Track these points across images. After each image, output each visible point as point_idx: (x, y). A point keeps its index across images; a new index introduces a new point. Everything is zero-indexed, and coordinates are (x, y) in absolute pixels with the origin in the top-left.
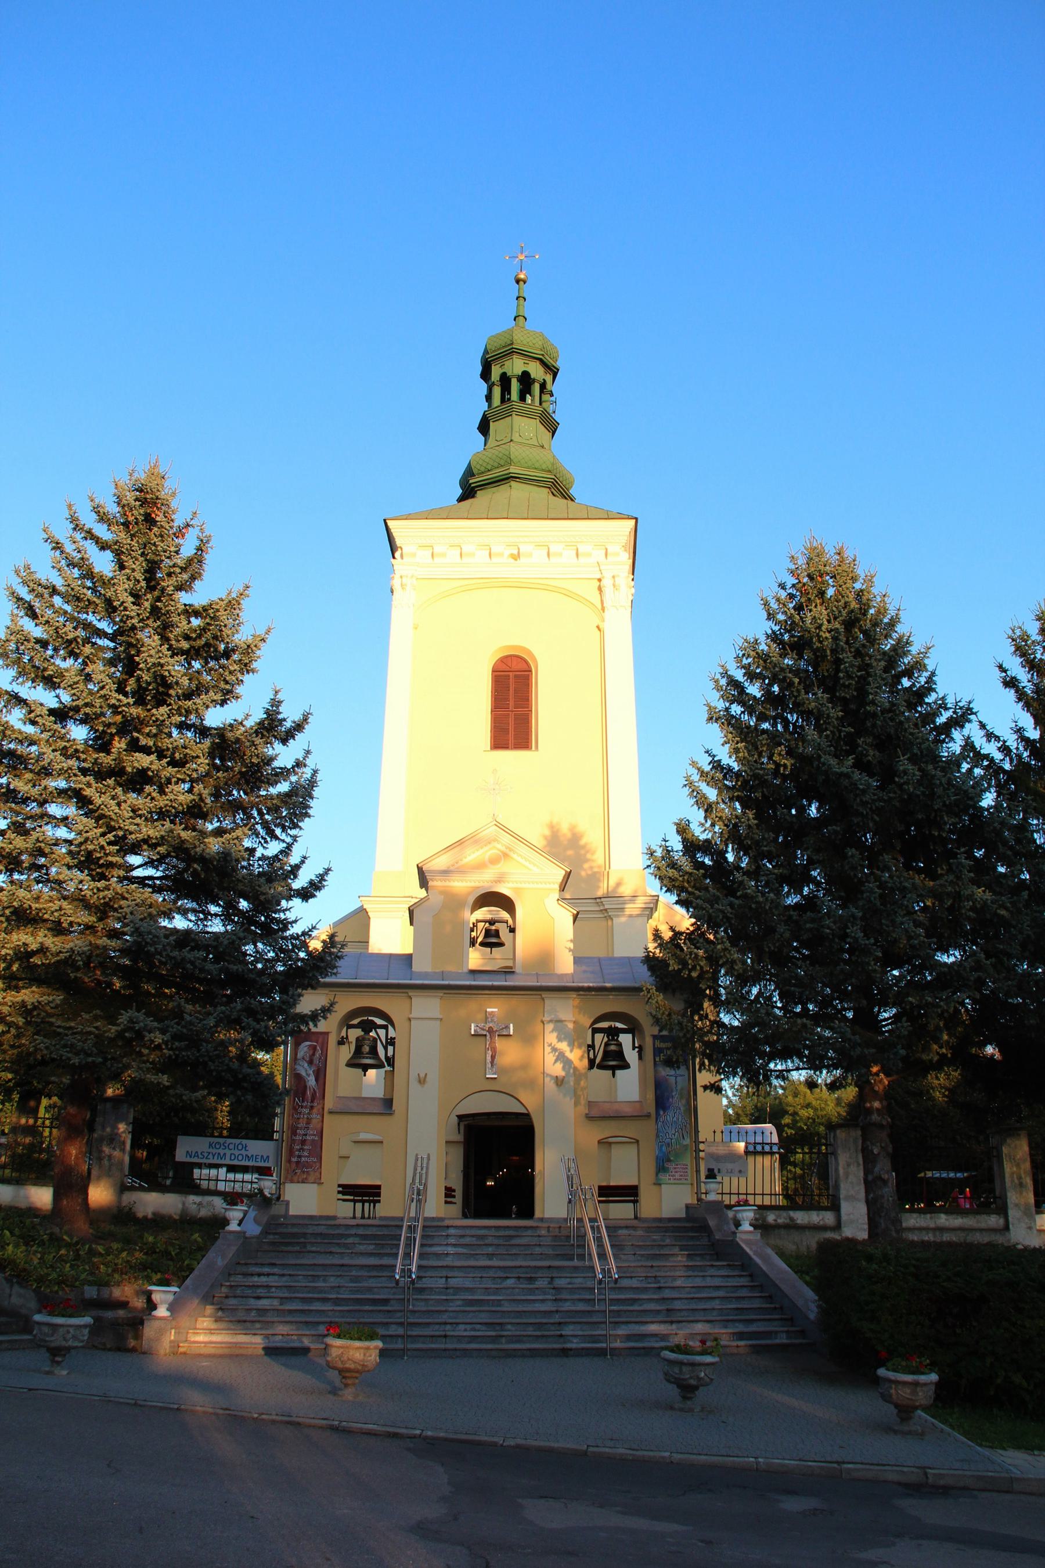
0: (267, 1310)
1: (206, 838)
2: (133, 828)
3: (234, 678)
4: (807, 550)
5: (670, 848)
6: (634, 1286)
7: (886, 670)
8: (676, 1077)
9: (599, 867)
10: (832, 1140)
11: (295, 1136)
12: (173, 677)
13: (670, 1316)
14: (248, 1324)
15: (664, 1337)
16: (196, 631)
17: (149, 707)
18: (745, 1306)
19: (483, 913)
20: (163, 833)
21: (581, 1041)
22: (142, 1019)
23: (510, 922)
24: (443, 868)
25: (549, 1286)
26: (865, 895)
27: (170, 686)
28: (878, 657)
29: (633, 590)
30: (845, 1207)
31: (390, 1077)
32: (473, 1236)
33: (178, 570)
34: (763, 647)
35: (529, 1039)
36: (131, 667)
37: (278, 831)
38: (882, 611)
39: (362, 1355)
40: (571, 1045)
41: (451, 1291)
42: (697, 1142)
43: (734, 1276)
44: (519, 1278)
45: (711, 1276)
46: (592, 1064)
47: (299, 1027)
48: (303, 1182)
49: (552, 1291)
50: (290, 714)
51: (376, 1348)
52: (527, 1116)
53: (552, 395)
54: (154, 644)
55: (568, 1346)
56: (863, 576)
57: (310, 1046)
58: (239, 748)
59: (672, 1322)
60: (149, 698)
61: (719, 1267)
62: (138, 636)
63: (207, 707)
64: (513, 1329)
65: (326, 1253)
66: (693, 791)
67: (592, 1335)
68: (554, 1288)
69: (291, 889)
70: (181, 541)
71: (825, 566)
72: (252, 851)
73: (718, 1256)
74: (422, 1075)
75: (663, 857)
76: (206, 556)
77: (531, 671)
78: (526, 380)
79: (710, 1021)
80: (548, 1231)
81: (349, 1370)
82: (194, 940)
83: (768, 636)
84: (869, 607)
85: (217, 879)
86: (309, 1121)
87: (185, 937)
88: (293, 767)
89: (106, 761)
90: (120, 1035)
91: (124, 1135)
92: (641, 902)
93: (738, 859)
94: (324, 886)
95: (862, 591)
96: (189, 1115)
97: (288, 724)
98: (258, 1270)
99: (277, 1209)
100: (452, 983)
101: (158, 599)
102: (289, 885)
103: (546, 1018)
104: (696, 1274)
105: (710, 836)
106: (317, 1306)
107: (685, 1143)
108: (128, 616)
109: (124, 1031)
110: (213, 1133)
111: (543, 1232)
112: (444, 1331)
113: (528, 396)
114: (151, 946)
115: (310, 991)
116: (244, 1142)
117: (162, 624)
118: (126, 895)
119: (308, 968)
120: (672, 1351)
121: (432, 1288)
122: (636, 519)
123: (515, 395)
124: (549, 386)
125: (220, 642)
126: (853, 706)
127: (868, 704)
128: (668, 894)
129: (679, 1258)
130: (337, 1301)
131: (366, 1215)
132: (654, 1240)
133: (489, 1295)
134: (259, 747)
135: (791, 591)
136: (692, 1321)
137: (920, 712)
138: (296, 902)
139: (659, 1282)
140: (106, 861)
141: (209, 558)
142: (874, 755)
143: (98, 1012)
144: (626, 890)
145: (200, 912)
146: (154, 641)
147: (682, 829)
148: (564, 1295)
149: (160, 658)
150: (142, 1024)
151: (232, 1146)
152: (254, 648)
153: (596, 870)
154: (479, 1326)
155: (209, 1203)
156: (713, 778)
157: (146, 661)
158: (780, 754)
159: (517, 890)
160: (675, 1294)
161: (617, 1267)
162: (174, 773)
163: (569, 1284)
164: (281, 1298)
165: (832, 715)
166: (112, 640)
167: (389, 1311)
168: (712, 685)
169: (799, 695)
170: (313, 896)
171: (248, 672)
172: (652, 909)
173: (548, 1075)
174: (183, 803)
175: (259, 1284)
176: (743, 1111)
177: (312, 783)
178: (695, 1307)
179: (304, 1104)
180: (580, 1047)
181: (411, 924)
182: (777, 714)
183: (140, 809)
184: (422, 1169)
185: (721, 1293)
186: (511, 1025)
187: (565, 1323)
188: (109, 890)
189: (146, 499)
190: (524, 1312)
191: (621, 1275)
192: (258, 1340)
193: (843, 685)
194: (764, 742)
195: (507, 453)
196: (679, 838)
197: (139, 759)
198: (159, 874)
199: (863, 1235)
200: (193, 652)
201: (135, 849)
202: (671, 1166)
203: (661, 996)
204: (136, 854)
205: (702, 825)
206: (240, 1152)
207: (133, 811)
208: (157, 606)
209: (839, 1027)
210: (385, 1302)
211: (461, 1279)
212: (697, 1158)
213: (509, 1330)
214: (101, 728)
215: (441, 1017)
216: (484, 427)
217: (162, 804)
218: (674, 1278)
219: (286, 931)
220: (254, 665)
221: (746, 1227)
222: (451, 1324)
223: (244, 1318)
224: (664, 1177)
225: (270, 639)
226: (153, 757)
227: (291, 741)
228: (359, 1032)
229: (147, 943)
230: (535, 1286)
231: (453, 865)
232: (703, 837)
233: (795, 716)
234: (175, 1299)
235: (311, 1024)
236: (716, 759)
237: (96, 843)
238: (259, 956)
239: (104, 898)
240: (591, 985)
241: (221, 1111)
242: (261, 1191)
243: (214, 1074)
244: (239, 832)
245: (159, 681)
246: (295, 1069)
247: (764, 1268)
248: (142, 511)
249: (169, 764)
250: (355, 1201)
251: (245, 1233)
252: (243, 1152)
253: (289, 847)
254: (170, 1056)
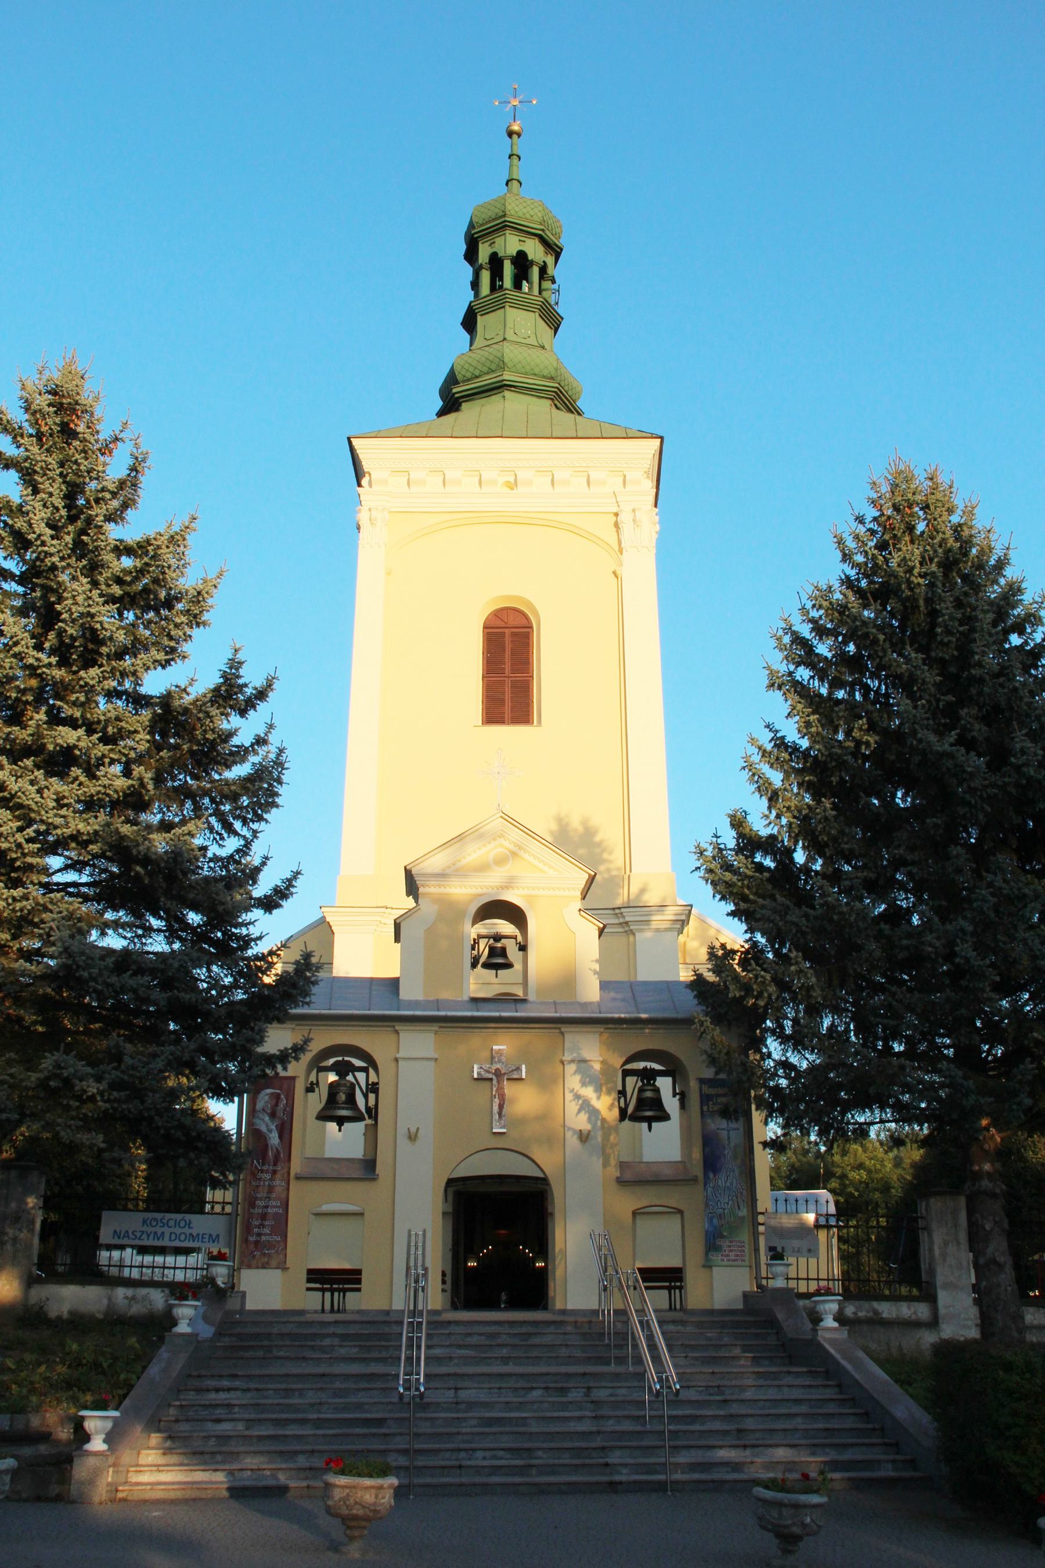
0: (230, 1437)
1: (152, 833)
2: (59, 821)
3: (181, 633)
4: (892, 474)
5: (722, 846)
6: (693, 1398)
7: (995, 624)
8: (729, 1131)
9: (618, 869)
10: (924, 1212)
11: (254, 1208)
12: (106, 630)
13: (741, 1438)
14: (207, 1457)
15: (737, 1467)
16: (131, 573)
17: (75, 668)
18: (836, 1426)
19: (481, 928)
20: (97, 827)
21: (609, 1085)
22: (74, 1065)
23: (520, 938)
24: (436, 871)
25: (586, 1399)
26: (975, 905)
27: (102, 642)
28: (986, 608)
29: (657, 528)
30: (943, 1297)
31: (372, 1135)
32: (481, 1334)
33: (108, 496)
34: (838, 596)
35: (548, 1082)
36: (49, 618)
37: (238, 825)
38: (986, 551)
39: (373, 1496)
40: (598, 1090)
41: (463, 1406)
42: (754, 1213)
43: (818, 1386)
44: (547, 1388)
45: (789, 1386)
46: (623, 1114)
47: (264, 1071)
48: (264, 1267)
49: (589, 1405)
50: (252, 677)
51: (390, 1486)
52: (545, 1180)
53: (554, 282)
54: (80, 590)
55: (617, 1478)
56: (961, 506)
57: (272, 1094)
58: (186, 720)
59: (745, 1447)
60: (74, 657)
61: (798, 1374)
62: (60, 579)
63: (148, 668)
64: (545, 1456)
65: (297, 1358)
66: (754, 775)
67: (645, 1464)
68: (592, 1402)
69: (251, 898)
70: (108, 459)
71: (914, 494)
72: (204, 849)
73: (791, 1360)
74: (413, 1130)
75: (714, 858)
76: (142, 479)
77: (531, 627)
78: (521, 261)
79: (774, 1060)
80: (576, 1327)
81: (356, 1518)
82: (135, 962)
83: (842, 582)
84: (972, 546)
85: (164, 885)
86: (271, 1189)
87: (124, 960)
88: (252, 745)
89: (21, 737)
90: (43, 1084)
91: (33, 1212)
92: (670, 914)
93: (810, 859)
94: (292, 894)
95: (960, 525)
96: (96, 1183)
97: (249, 691)
98: (212, 1383)
99: (232, 1304)
100: (450, 1013)
101: (83, 532)
102: (249, 893)
103: (567, 1057)
104: (769, 1382)
105: (775, 831)
106: (291, 1430)
107: (741, 1214)
108: (46, 553)
109: (48, 1079)
110: (126, 1205)
111: (569, 1328)
112: (457, 1459)
113: (525, 283)
114: (84, 970)
115: (275, 1025)
116: (188, 1217)
117: (90, 563)
118: (50, 906)
119: (278, 996)
120: (767, 1487)
121: (438, 1404)
122: (662, 438)
123: (508, 282)
124: (550, 271)
125: (162, 587)
126: (953, 670)
127: (974, 667)
128: (723, 902)
129: (742, 1362)
130: (319, 1423)
131: (336, 1308)
132: (710, 1339)
133: (510, 1411)
134: (215, 719)
135: (871, 526)
136: (771, 1446)
137: (1036, 677)
138: (257, 914)
139: (723, 1394)
140: (24, 863)
141: (146, 480)
142: (980, 730)
143: (12, 1055)
144: (652, 898)
145: (138, 927)
146: (82, 585)
147: (738, 822)
148: (606, 1411)
149: (89, 606)
150: (71, 1070)
151: (172, 1223)
152: (206, 595)
153: (614, 873)
154: (501, 1453)
155: (145, 1298)
156: (777, 759)
157: (70, 609)
158: (860, 729)
159: (529, 898)
160: (743, 1410)
161: (677, 1374)
162: (106, 752)
163: (611, 1395)
164: (248, 1420)
165: (928, 680)
166: (19, 583)
167: (385, 1435)
168: (773, 643)
169: (885, 656)
170: (278, 906)
171: (198, 625)
172: (683, 921)
173: (569, 1129)
174: (119, 789)
175: (219, 1402)
176: (776, 1173)
177: (279, 764)
178: (772, 1427)
179: (265, 1168)
180: (609, 1093)
181: (397, 939)
182: (855, 679)
183: (64, 797)
184: (416, 1249)
185: (803, 1409)
186: (524, 1067)
187: (612, 1448)
188: (28, 899)
189: (62, 404)
190: (558, 1433)
191: (685, 1384)
192: (220, 1477)
193: (942, 643)
194: (841, 714)
195: (499, 355)
196: (734, 833)
197: (63, 734)
198: (84, 879)
199: (974, 1333)
200: (127, 599)
201: (52, 849)
202: (725, 1244)
203: (718, 1030)
204: (56, 854)
205: (767, 817)
206: (183, 1230)
207: (57, 801)
208: (83, 541)
209: (949, 1069)
210: (380, 1422)
211: (474, 1391)
212: (755, 1235)
213: (540, 1458)
214: (14, 695)
215: (436, 1056)
216: (469, 323)
217: (93, 790)
218: (743, 1388)
219: (246, 949)
220: (206, 617)
221: (829, 1322)
222: (466, 1450)
223: (201, 1449)
224: (716, 1258)
225: (222, 584)
226: (81, 732)
227: (252, 712)
228: (332, 1077)
229: (78, 967)
230: (570, 1399)
231: (449, 867)
232: (764, 832)
233: (877, 683)
234: (115, 1426)
235: (279, 1067)
236: (778, 735)
237: (12, 840)
238: (215, 983)
239: (21, 910)
240: (623, 1016)
241: (136, 1177)
242: (212, 1280)
243: (162, 1132)
244: (191, 826)
245: (88, 635)
246: (253, 1124)
247: (857, 1376)
248: (58, 420)
249: (100, 740)
250: (323, 1290)
251: (197, 1335)
252: (187, 1231)
253: (248, 844)
254: (107, 1110)
